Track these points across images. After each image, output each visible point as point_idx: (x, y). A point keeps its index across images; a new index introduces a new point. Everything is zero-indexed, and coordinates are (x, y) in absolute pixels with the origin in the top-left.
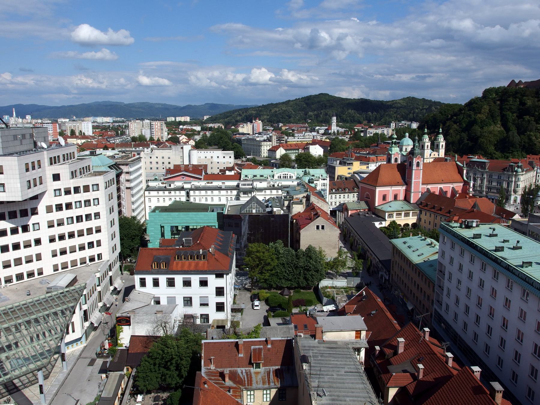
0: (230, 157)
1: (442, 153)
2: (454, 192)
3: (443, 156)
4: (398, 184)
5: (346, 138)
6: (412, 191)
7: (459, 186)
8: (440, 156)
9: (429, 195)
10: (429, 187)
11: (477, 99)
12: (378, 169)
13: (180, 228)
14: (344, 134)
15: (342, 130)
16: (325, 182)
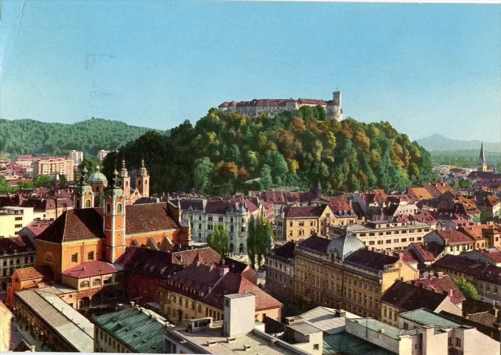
0: (291, 234)
1: (146, 193)
3: (148, 196)
7: (169, 234)
8: (144, 196)
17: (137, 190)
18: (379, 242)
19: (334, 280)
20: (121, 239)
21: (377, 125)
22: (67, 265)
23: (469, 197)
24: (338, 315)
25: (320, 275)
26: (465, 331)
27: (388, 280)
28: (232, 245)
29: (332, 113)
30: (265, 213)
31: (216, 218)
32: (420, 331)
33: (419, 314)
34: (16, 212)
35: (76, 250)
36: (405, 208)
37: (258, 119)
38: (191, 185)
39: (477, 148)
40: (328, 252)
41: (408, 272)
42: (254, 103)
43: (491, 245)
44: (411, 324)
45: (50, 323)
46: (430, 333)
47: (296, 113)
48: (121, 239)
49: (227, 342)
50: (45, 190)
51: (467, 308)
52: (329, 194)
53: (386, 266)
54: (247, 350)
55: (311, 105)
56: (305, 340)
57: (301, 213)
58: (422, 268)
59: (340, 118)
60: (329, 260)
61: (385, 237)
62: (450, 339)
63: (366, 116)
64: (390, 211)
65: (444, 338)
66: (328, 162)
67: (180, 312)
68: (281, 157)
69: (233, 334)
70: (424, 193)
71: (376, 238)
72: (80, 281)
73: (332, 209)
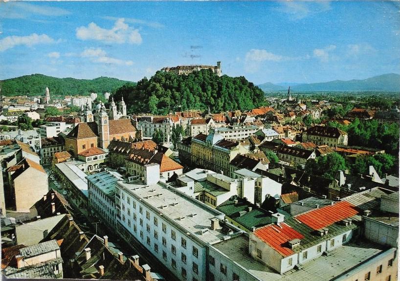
6: (103, 140)
7: (133, 135)
16: (38, 139)
17: (120, 113)
18: (230, 136)
19: (208, 155)
20: (107, 137)
21: (238, 78)
22: (80, 151)
23: (281, 113)
24: (204, 172)
25: (203, 152)
26: (263, 179)
27: (233, 155)
28: (166, 138)
29: (216, 72)
30: (184, 123)
31: (157, 125)
32: (241, 179)
33: (244, 171)
34: (57, 125)
35: (85, 142)
36: (249, 119)
37: (180, 76)
38: (147, 110)
39: (397, 91)
40: (206, 141)
41: (243, 150)
42: (178, 68)
43: (287, 136)
44: (239, 176)
45: (70, 179)
46: (245, 180)
47: (198, 72)
48: (107, 137)
49: (145, 187)
50: (76, 113)
51: (271, 167)
52: (214, 113)
53: (232, 148)
54: (154, 191)
55: (206, 69)
56: (186, 185)
57: (199, 122)
58: (284, 191)
59: (220, 75)
60: (207, 145)
61: (237, 133)
62: (256, 183)
63: (233, 74)
64: (242, 120)
65: (253, 182)
66: (214, 97)
67: (135, 171)
68: (191, 95)
69: (148, 183)
70: (260, 112)
71: (234, 134)
72: (87, 158)
73: (214, 120)
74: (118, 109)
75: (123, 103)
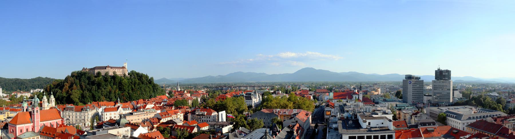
2: (57, 124)
4: (28, 123)
5: (7, 100)
9: (45, 127)
10: (44, 122)
11: (68, 76)
12: (17, 115)
13: (225, 100)
14: (6, 97)
15: (5, 95)
73: (122, 108)
74: (48, 100)
75: (52, 97)
